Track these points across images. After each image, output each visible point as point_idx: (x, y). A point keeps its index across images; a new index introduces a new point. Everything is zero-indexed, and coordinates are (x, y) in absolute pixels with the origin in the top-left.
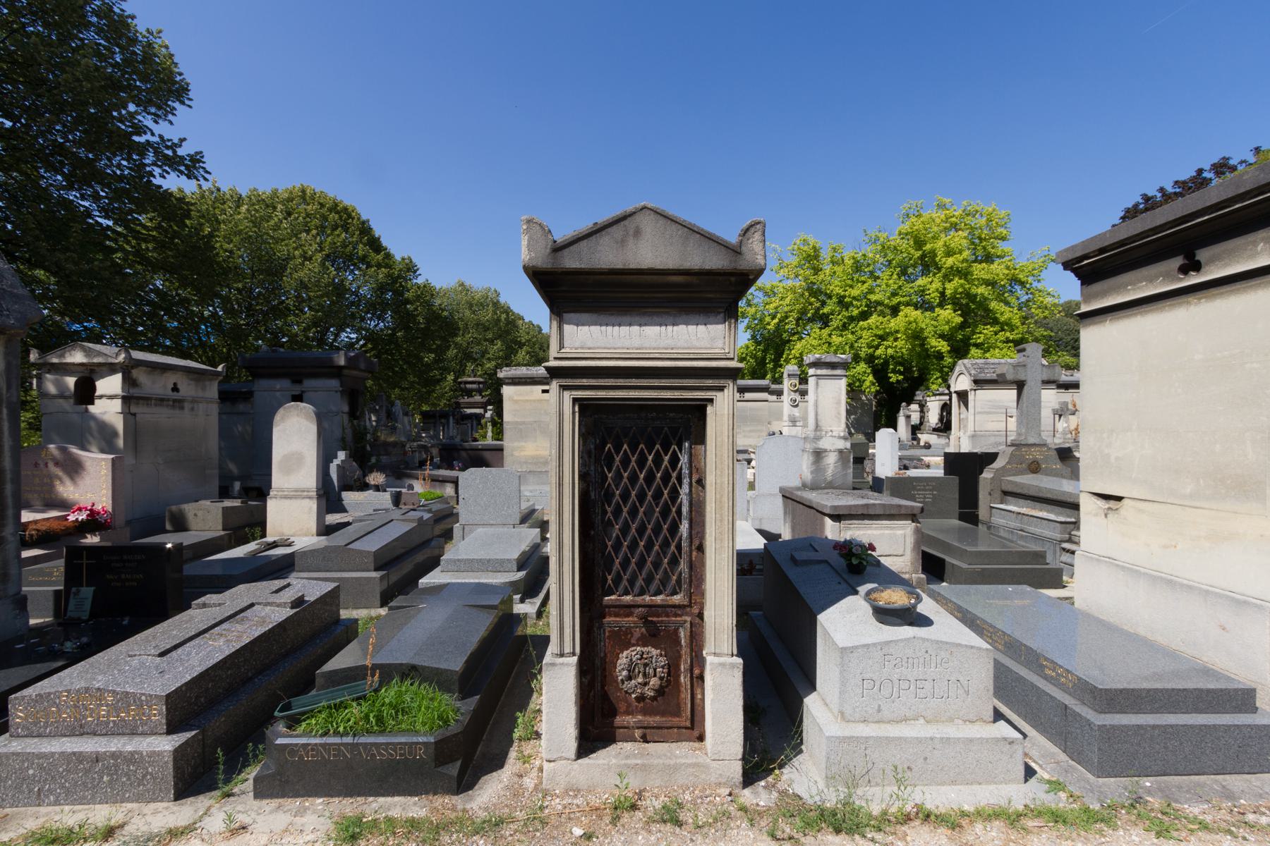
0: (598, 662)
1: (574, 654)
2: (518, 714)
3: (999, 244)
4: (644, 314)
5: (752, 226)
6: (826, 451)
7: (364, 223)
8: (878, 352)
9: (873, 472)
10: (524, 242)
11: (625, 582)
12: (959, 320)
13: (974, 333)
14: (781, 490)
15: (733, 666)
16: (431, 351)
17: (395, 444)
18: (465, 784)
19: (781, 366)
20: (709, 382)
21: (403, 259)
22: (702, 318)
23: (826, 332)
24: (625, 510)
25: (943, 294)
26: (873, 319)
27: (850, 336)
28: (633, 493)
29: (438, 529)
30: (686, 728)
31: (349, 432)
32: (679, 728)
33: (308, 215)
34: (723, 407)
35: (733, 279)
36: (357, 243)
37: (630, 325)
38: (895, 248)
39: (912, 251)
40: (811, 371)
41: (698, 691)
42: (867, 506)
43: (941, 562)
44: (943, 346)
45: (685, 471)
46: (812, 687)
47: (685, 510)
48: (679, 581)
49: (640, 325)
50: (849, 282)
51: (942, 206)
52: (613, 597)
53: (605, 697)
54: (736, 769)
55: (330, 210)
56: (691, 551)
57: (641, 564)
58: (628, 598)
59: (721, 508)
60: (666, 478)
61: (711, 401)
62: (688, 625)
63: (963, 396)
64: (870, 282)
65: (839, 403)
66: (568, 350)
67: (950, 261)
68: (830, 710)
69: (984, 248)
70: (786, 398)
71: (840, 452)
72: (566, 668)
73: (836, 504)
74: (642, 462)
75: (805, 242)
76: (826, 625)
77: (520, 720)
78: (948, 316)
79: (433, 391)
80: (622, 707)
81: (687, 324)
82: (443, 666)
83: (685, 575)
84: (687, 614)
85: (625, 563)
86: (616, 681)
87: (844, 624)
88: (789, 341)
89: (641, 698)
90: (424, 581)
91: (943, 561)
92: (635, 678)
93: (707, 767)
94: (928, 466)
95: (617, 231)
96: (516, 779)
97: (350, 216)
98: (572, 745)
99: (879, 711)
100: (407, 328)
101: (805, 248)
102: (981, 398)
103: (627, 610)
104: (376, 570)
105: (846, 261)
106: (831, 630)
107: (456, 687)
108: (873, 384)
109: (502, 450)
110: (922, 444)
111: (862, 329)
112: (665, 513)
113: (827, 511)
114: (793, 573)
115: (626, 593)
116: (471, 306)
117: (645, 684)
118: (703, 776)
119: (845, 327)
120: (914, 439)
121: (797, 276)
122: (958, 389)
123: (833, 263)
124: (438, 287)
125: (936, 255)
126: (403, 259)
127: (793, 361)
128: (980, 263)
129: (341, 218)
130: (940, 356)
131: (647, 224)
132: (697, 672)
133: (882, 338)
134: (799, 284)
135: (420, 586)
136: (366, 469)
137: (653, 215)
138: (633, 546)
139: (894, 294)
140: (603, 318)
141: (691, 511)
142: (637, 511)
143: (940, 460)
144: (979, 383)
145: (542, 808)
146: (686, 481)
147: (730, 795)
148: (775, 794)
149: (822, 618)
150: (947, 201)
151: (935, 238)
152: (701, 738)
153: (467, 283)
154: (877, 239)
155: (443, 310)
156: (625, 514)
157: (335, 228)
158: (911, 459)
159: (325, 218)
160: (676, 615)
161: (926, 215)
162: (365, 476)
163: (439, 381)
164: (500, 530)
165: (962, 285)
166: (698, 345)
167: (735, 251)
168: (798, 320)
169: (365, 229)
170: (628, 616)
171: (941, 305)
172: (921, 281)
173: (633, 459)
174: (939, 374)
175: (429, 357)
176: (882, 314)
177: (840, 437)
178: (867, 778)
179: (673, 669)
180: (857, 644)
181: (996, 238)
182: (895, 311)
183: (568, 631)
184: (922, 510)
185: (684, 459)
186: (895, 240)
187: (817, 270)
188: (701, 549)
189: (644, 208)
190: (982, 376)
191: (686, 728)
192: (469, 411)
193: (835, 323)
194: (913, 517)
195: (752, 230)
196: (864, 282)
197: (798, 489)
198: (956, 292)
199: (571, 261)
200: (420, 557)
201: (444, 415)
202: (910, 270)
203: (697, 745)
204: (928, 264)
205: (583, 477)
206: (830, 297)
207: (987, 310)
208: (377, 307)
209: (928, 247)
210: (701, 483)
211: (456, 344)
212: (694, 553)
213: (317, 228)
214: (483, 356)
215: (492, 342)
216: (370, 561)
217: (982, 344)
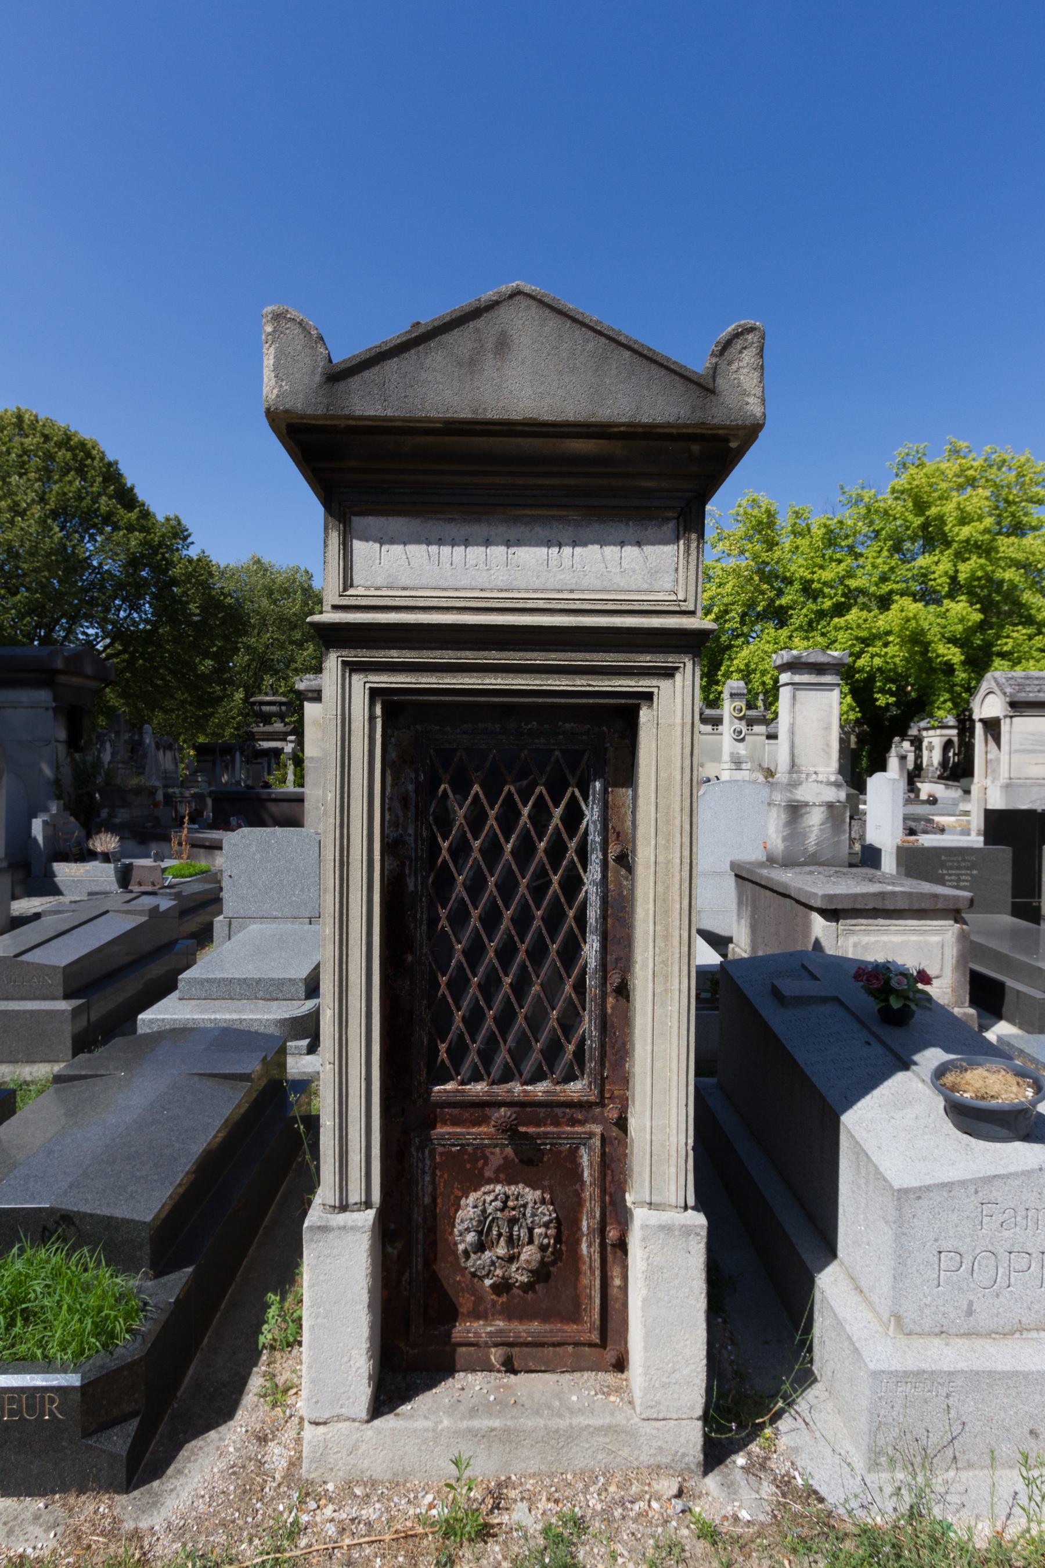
0: (418, 1216)
1: (368, 1204)
2: (271, 1297)
3: (1032, 508)
4: (515, 520)
5: (737, 335)
6: (806, 804)
7: (110, 465)
8: (860, 663)
9: (862, 837)
10: (269, 361)
11: (473, 1057)
12: (978, 617)
13: (999, 637)
14: (733, 866)
15: (687, 1231)
16: (206, 655)
17: (138, 791)
18: (143, 1466)
19: (717, 683)
20: (646, 660)
21: (168, 519)
22: (632, 530)
23: (784, 632)
24: (475, 913)
25: (954, 579)
26: (854, 615)
27: (819, 639)
28: (492, 881)
29: (193, 924)
30: (591, 1345)
31: (67, 771)
32: (577, 1344)
33: (26, 452)
34: (671, 704)
35: (696, 448)
36: (99, 495)
37: (487, 543)
38: (886, 513)
39: (910, 517)
40: (784, 678)
41: (615, 1271)
42: (882, 895)
43: (998, 988)
44: (954, 655)
45: (595, 838)
46: (829, 1251)
47: (593, 914)
48: (580, 1054)
49: (508, 544)
50: (819, 561)
51: (956, 452)
52: (450, 1086)
53: (433, 1284)
54: (691, 1437)
55: (59, 445)
56: (604, 996)
57: (506, 1019)
58: (479, 1088)
59: (666, 912)
60: (556, 851)
61: (648, 697)
62: (597, 1142)
63: (992, 726)
64: (849, 560)
65: (828, 728)
66: (361, 591)
67: (965, 531)
68: (870, 1305)
69: (1013, 515)
70: (727, 728)
71: (830, 806)
72: (350, 1237)
73: (831, 891)
74: (509, 818)
75: (755, 503)
76: (860, 1134)
77: (273, 1311)
78: (961, 611)
79: (212, 714)
80: (465, 1303)
81: (603, 543)
82: (119, 1213)
83: (592, 1043)
84: (594, 1120)
85: (474, 1021)
86: (454, 1252)
87: (894, 1134)
88: (730, 647)
89: (503, 1287)
90: (151, 1018)
91: (1001, 986)
92: (492, 1245)
93: (632, 1434)
94: (942, 830)
95: (460, 340)
96: (253, 1447)
97: (88, 455)
98: (362, 1392)
99: (970, 1312)
100: (173, 621)
101: (755, 512)
102: (1020, 730)
103: (478, 1112)
104: (67, 997)
105: (814, 530)
106: (870, 1146)
107: (145, 1254)
108: (852, 709)
109: (302, 800)
110: (923, 796)
111: (837, 629)
112: (554, 918)
113: (818, 904)
114: (777, 1020)
115: (476, 1078)
116: (271, 593)
117: (512, 1259)
118: (625, 1452)
119: (811, 626)
120: (911, 790)
121: (742, 552)
122: (982, 716)
123: (795, 533)
124: (140, 499)
125: (944, 523)
126: (168, 519)
127: (735, 676)
128: (1008, 535)
129: (75, 456)
130: (949, 669)
131: (523, 325)
132: (612, 1234)
133: (867, 642)
134: (745, 563)
135: (141, 1030)
136: (91, 827)
137: (534, 310)
138: (490, 986)
139: (884, 579)
140: (433, 527)
141: (604, 917)
142: (499, 916)
143: (977, 822)
144: (1018, 707)
145: (295, 1531)
146: (595, 858)
147: (679, 1494)
148: (768, 1489)
149: (852, 1120)
150: (963, 444)
151: (944, 498)
152: (620, 1365)
153: (265, 560)
154: (859, 499)
155: (226, 596)
156: (474, 921)
157: (66, 471)
158: (917, 819)
159: (50, 457)
160: (574, 1122)
161: (930, 467)
162: (89, 836)
163: (220, 699)
164: (288, 927)
165: (982, 567)
166: (623, 584)
167: (704, 387)
168: (743, 615)
169: (111, 475)
170: (477, 1123)
171: (951, 595)
172: (923, 561)
173: (492, 814)
174: (947, 696)
175: (208, 665)
176: (865, 607)
177: (830, 784)
178: (949, 1452)
179: (565, 1229)
180: (928, 1181)
181: (1030, 500)
182: (884, 603)
183: (356, 1158)
184: (972, 902)
185: (591, 814)
186: (887, 500)
187: (771, 544)
188: (623, 991)
189: (517, 293)
190: (1022, 696)
191: (591, 1345)
192: (266, 745)
193: (797, 619)
194: (955, 914)
195: (739, 344)
196: (840, 561)
197: (762, 865)
198: (973, 577)
199: (365, 402)
200: (156, 970)
201: (227, 750)
202: (907, 545)
203: (611, 1378)
204: (933, 536)
205: (389, 847)
206: (790, 582)
207: (1018, 605)
208: (130, 590)
209: (933, 511)
210: (625, 861)
211: (248, 648)
212: (611, 1000)
213: (38, 470)
214: (288, 667)
215: (300, 644)
216: (57, 984)
217: (1011, 653)
